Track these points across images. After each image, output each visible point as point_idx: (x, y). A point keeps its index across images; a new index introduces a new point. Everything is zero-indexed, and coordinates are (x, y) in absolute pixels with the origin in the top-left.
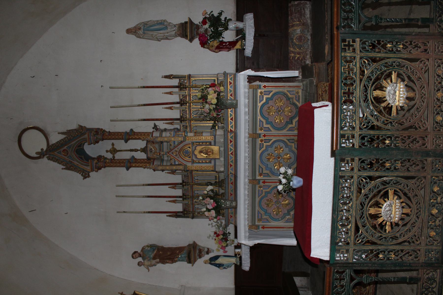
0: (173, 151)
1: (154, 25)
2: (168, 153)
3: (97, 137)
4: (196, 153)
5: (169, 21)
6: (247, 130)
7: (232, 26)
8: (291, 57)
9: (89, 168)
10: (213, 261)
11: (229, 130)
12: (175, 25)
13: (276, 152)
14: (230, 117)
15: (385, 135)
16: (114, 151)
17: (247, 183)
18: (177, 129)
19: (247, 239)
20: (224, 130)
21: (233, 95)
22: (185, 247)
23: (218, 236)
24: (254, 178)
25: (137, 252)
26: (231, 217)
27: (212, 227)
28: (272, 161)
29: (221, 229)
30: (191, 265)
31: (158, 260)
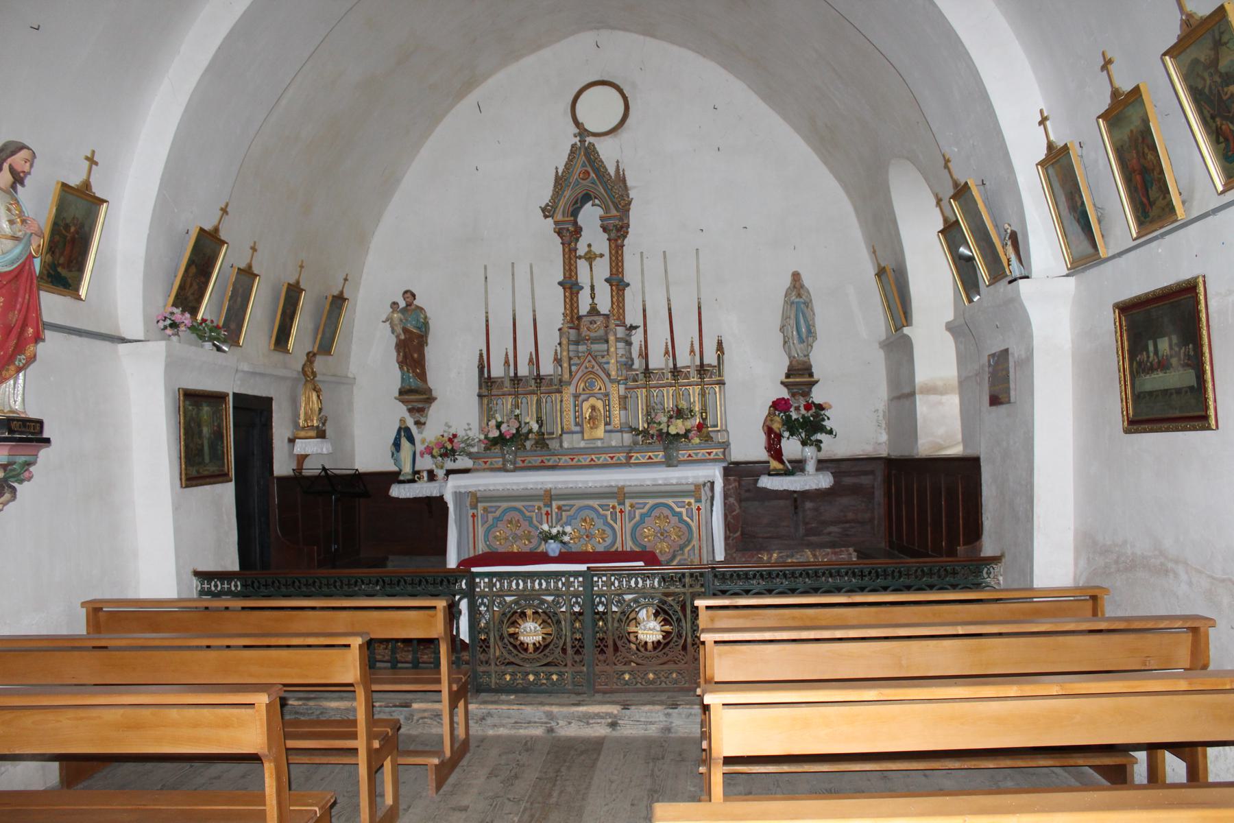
0: (593, 363)
1: (806, 321)
2: (589, 354)
3: (612, 230)
4: (592, 401)
5: (815, 345)
6: (628, 483)
7: (809, 452)
8: (762, 554)
9: (559, 217)
10: (405, 433)
11: (633, 454)
12: (808, 355)
13: (597, 532)
14: (654, 455)
15: (607, 621)
16: (590, 257)
17: (546, 487)
18: (633, 364)
19: (454, 490)
20: (632, 445)
21: (690, 458)
22: (427, 384)
23: (451, 440)
24: (553, 497)
25: (415, 299)
26: (486, 463)
27: (465, 430)
28: (582, 525)
29: (462, 445)
30: (397, 394)
31: (402, 337)
